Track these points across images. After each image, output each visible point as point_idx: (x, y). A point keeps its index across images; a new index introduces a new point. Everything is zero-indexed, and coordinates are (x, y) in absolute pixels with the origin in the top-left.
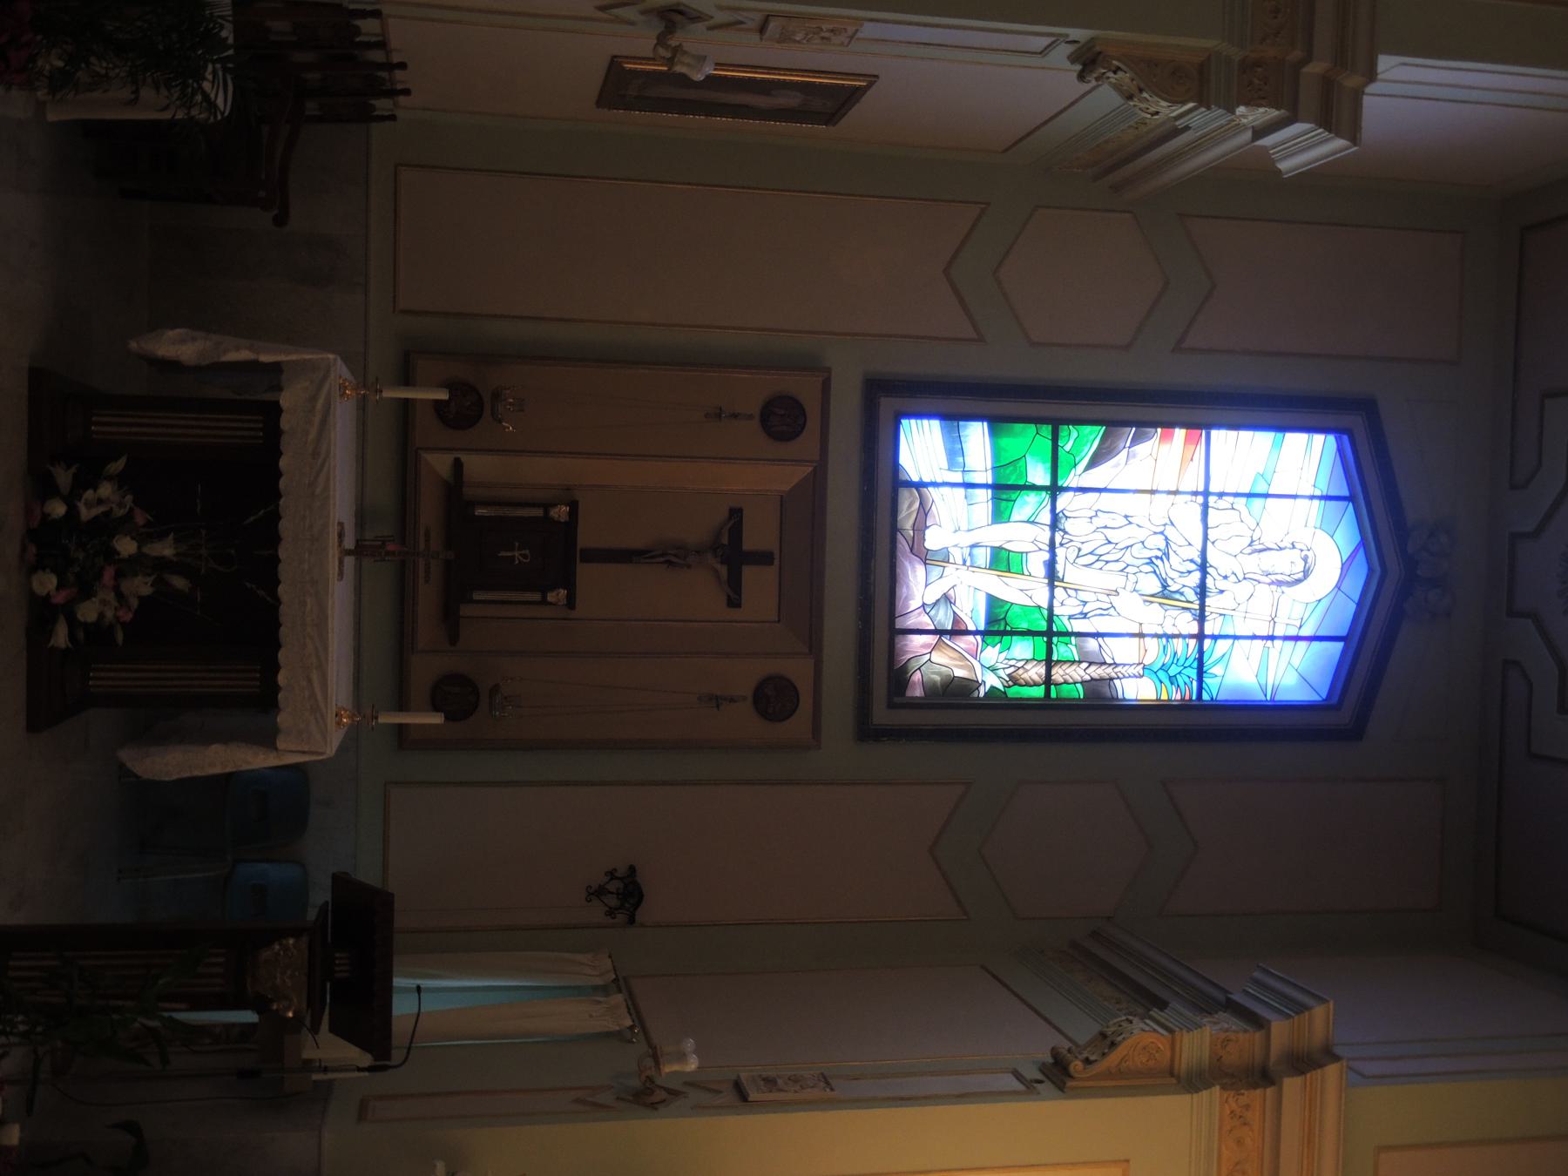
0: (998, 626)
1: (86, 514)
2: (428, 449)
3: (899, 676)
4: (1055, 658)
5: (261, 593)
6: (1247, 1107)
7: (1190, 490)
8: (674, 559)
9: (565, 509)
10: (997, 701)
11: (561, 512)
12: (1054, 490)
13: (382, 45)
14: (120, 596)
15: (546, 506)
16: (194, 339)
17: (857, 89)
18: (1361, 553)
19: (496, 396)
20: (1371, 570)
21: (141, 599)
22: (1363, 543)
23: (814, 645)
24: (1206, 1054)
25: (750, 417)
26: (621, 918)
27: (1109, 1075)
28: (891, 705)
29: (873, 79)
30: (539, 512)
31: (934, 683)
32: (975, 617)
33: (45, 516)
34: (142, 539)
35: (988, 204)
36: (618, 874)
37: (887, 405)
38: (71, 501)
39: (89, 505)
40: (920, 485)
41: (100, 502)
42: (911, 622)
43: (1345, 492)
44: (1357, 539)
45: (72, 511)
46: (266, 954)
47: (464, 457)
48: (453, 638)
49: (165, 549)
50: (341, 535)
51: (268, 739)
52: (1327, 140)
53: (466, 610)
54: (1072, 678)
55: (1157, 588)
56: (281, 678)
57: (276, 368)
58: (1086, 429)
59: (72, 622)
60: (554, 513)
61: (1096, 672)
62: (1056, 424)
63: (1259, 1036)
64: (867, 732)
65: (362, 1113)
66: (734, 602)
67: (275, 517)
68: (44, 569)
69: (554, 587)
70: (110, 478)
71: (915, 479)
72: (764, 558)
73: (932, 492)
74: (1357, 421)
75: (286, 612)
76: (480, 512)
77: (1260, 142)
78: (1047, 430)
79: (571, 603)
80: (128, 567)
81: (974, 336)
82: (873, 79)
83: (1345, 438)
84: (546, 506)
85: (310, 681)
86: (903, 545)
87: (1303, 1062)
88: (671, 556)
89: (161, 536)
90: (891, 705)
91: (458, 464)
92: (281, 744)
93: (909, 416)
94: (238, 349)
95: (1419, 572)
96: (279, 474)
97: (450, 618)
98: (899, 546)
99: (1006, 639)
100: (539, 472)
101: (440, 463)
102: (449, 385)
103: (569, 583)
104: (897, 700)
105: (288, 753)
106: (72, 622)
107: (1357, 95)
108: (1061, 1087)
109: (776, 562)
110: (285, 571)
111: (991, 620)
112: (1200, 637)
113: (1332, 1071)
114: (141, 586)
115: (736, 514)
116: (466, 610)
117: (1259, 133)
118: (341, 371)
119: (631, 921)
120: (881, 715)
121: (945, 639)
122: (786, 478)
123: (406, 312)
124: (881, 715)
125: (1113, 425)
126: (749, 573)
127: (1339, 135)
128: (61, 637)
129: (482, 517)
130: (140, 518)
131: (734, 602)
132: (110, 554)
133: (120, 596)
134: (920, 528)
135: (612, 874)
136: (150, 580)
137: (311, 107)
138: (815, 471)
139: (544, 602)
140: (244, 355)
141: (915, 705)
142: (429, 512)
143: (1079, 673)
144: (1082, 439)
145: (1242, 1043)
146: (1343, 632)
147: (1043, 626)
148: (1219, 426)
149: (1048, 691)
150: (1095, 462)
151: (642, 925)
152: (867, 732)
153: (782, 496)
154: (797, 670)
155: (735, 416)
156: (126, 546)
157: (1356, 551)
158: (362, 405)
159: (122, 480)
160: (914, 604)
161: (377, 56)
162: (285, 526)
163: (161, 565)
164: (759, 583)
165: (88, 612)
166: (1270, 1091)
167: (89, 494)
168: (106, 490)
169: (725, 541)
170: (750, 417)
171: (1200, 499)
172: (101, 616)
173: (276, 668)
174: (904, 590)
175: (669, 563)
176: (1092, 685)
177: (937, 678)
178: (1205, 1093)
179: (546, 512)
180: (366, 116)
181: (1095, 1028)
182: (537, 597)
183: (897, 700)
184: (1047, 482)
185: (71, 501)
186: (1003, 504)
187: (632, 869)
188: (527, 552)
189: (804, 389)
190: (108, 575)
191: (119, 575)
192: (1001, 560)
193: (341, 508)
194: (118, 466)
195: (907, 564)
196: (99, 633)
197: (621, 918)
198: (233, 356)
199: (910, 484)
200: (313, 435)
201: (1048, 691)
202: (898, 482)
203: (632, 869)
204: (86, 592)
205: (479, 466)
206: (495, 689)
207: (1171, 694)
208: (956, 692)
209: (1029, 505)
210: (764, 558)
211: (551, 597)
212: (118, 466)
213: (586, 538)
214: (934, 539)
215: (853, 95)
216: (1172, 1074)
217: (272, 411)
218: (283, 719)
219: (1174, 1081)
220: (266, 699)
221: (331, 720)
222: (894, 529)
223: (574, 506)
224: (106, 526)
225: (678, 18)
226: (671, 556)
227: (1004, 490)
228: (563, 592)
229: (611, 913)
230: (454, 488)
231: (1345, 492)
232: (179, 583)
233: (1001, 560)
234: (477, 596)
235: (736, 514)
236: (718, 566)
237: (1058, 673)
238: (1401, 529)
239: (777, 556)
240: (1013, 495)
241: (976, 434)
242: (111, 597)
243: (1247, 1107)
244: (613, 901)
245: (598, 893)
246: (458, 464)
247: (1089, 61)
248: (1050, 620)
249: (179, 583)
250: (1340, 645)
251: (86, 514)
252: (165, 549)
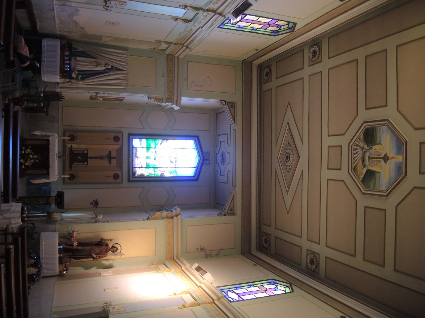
0: (147, 167)
1: (26, 153)
2: (67, 144)
3: (134, 173)
4: (156, 171)
5: (47, 162)
6: (170, 221)
7: (157, 149)
8: (101, 158)
9: (86, 151)
10: (148, 177)
11: (86, 152)
12: (155, 148)
13: (61, 95)
14: (30, 162)
15: (84, 151)
16: (39, 132)
17: (122, 99)
18: (198, 156)
19: (76, 137)
20: (199, 158)
21: (32, 163)
22: (198, 155)
23: (121, 169)
24: (165, 215)
25: (112, 139)
26: (95, 207)
27: (154, 218)
28: (133, 177)
29: (124, 98)
30: (83, 152)
31: (139, 175)
32: (145, 166)
33: (22, 153)
34: (33, 155)
35: (145, 110)
36: (95, 201)
37: (131, 137)
38: (25, 151)
39: (27, 152)
40: (136, 148)
41: (28, 151)
42: (175, 176)
43: (195, 148)
44: (197, 154)
45: (25, 152)
46: (50, 199)
47: (72, 145)
48: (71, 169)
49: (36, 157)
50: (57, 155)
51: (48, 178)
52: (177, 107)
53: (73, 165)
54: (158, 174)
55: (170, 161)
56: (50, 171)
57: (49, 135)
58: (159, 140)
59: (25, 165)
60: (85, 152)
61: (162, 172)
62: (155, 139)
63: (172, 213)
64: (129, 181)
65: (60, 224)
66: (110, 164)
67: (49, 153)
68: (22, 159)
69: (85, 162)
70: (29, 148)
71: (136, 147)
72: (114, 158)
73: (137, 148)
74: (196, 139)
75: (50, 164)
76: (75, 152)
77: (171, 106)
78: (154, 140)
79: (87, 164)
80: (31, 159)
81: (143, 128)
82: (124, 98)
83: (195, 141)
84: (84, 151)
85: (53, 172)
86: (134, 156)
87: (177, 215)
88: (101, 158)
89: (35, 155)
90: (133, 177)
91: (71, 146)
92: (50, 179)
93: (134, 138)
94: (44, 133)
95: (205, 158)
96: (49, 148)
97: (70, 166)
98: (134, 156)
99: (149, 168)
100: (83, 146)
101: (69, 146)
102: (70, 175)
103: (87, 161)
104: (133, 177)
105: (51, 180)
106: (25, 165)
107: (180, 102)
108: (148, 220)
109: (116, 158)
110: (50, 159)
111: (147, 166)
112: (176, 167)
113: (180, 216)
114: (32, 161)
115: (110, 152)
116: (73, 165)
117: (171, 105)
118: (57, 135)
119: (97, 207)
120: (131, 179)
121: (140, 168)
122: (117, 147)
123: (64, 126)
124: (131, 179)
125: (163, 139)
126: (112, 160)
127: (178, 107)
128: (23, 167)
129: (75, 153)
130: (32, 153)
131: (110, 164)
132: (29, 157)
133: (30, 162)
134: (136, 153)
135: (94, 201)
136: (34, 160)
137: (51, 100)
138: (121, 146)
139: (84, 164)
140: (45, 134)
141: (136, 177)
142: (67, 152)
143: (160, 173)
144: (159, 141)
145: (170, 214)
146: (196, 167)
147: (154, 167)
148: (177, 139)
149: (155, 175)
150: (161, 144)
151: (98, 208)
152: (129, 181)
153: (117, 150)
154: (119, 173)
155: (110, 139)
156: (31, 156)
157: (197, 156)
158: (58, 139)
159: (30, 149)
160: (136, 164)
161: (61, 96)
162: (50, 154)
163: (35, 159)
164: (114, 161)
165: (27, 164)
166: (173, 219)
167: (27, 150)
168: (29, 150)
169: (109, 155)
170: (112, 139)
171: (175, 149)
172: (28, 164)
173: (49, 170)
174: (134, 162)
175: (101, 158)
176: (161, 174)
177: (140, 174)
178: (165, 219)
179: (84, 152)
180: (58, 100)
181: (153, 214)
182: (83, 163)
183: (133, 177)
184: (154, 147)
185: (25, 151)
186: (148, 150)
187: (97, 200)
188: (81, 157)
189: (120, 135)
190: (29, 160)
191: (30, 160)
192: (148, 158)
193: (57, 152)
194: (30, 147)
195: (135, 158)
196: (27, 167)
197: (95, 207)
198: (44, 134)
199: (135, 148)
200: (53, 143)
201: (155, 175)
202: (133, 147)
203: (97, 200)
204: (26, 162)
205: (74, 146)
206: (77, 176)
207: (172, 175)
208: (142, 176)
209: (152, 151)
210: (114, 158)
211: (85, 163)
212: (30, 147)
213: (90, 155)
214: (138, 155)
215: (123, 99)
216: (162, 218)
217: (48, 140)
218: (50, 176)
219: (162, 219)
220: (48, 174)
221: (56, 176)
222: (133, 153)
223: (87, 151)
224: (29, 154)
225: (98, 93)
226: (101, 158)
227: (148, 148)
228: (86, 163)
229: (94, 206)
230: (71, 149)
231: (195, 148)
232: (37, 161)
233: (148, 158)
234: (74, 163)
235: (110, 152)
236: (108, 159)
237: (156, 173)
238: (202, 153)
239: (116, 157)
240: (149, 149)
241: (144, 141)
242: (29, 162)
243: (170, 221)
244: (94, 204)
245: (92, 203)
246: (71, 146)
247: (149, 98)
248: (155, 166)
249: (37, 161)
250: (195, 168)
251: (26, 153)
252: (36, 157)
